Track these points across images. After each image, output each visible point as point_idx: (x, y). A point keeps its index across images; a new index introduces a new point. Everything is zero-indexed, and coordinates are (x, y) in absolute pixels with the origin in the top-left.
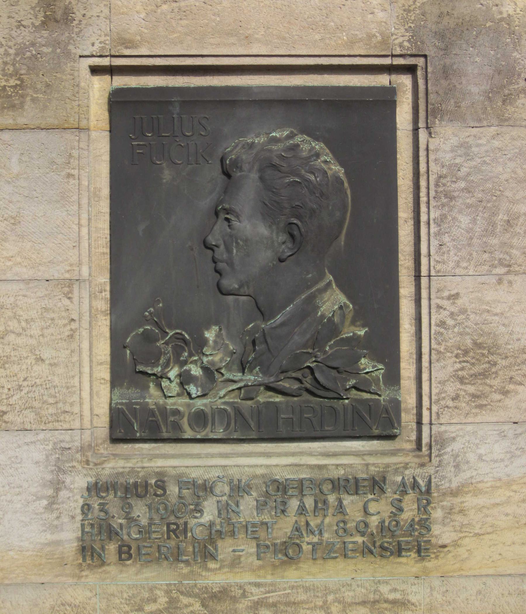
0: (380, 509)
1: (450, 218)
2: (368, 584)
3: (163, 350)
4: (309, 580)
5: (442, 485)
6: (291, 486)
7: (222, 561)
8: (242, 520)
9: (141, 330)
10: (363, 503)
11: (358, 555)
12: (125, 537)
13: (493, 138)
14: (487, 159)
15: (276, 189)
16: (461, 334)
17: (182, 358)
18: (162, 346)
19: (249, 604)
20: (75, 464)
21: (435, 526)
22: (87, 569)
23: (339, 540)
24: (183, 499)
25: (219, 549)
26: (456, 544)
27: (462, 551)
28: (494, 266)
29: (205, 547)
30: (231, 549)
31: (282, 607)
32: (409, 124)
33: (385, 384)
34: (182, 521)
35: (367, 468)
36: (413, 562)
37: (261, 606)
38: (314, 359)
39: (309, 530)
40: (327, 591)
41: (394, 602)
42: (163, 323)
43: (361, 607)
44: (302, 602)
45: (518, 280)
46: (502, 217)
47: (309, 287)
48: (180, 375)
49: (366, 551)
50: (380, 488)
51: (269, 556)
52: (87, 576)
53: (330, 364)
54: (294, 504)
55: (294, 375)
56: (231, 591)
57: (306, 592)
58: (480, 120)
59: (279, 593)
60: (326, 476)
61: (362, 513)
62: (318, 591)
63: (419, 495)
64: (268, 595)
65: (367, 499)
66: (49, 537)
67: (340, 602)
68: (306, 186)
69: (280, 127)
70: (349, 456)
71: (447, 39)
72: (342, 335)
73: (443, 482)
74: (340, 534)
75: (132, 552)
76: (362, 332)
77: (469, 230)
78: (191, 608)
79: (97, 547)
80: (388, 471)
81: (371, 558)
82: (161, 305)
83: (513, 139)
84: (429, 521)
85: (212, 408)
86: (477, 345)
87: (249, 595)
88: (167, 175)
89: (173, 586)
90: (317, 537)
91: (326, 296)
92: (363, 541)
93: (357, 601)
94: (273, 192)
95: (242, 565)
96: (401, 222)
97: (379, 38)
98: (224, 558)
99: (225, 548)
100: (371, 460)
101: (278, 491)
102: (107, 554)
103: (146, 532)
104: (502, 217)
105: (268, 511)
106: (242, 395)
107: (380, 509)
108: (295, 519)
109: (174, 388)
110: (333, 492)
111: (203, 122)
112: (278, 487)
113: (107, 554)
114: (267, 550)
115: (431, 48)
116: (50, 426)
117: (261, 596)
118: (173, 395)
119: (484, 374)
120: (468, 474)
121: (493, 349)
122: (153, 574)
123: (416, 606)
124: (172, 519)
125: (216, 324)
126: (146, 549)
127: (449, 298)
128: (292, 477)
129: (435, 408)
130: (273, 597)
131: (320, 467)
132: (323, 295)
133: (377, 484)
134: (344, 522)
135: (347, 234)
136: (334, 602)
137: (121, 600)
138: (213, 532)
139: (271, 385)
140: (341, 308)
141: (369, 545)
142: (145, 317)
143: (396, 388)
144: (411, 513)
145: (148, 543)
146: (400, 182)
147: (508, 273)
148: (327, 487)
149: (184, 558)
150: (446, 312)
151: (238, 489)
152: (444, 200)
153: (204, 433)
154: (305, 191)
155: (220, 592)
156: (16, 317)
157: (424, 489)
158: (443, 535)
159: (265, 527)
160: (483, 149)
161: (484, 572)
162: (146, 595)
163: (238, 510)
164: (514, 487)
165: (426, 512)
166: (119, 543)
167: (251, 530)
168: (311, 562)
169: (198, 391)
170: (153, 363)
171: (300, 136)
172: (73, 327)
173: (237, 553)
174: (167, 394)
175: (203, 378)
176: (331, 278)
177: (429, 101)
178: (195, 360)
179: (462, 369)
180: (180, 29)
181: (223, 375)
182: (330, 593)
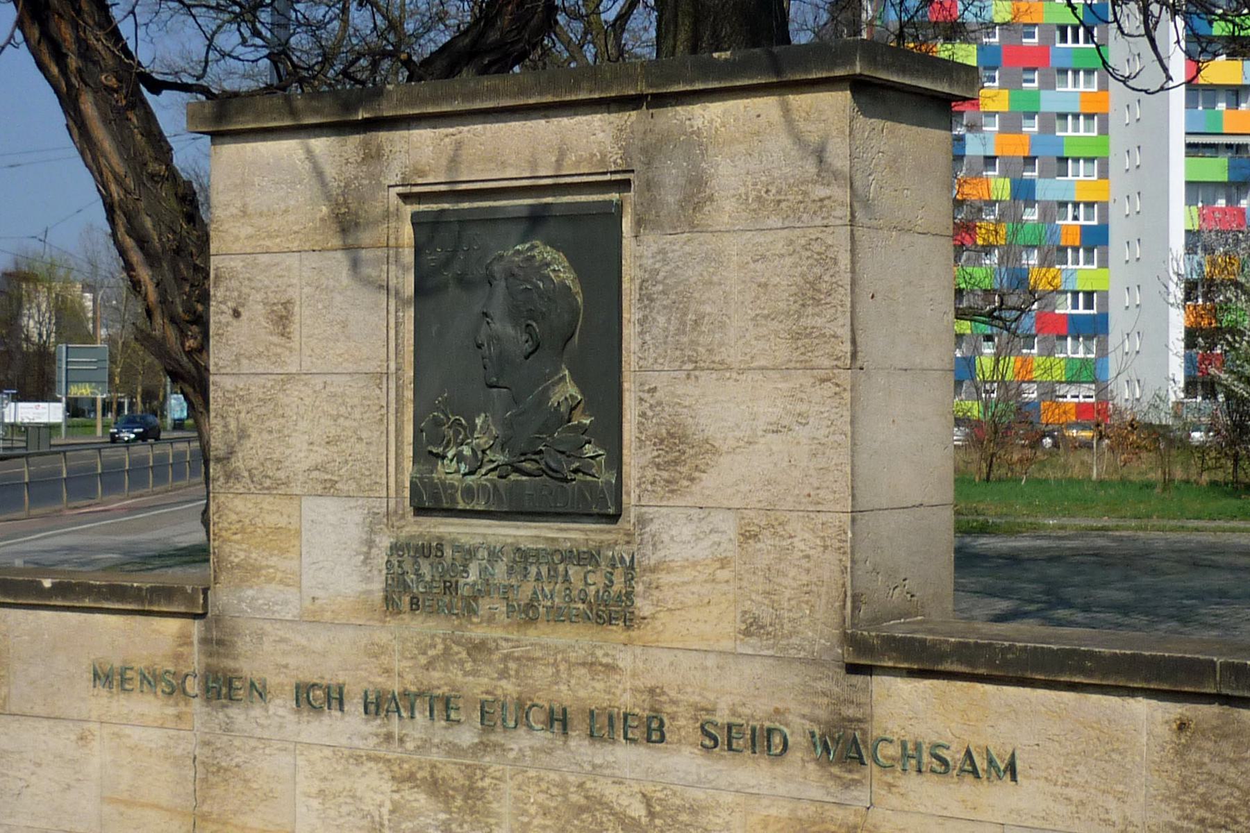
4: (545, 640)
13: (685, 244)
14: (680, 264)
16: (658, 424)
26: (653, 617)
27: (658, 624)
28: (683, 362)
34: (454, 580)
40: (558, 651)
41: (607, 666)
45: (703, 375)
46: (691, 316)
58: (675, 228)
66: (364, 586)
77: (666, 330)
83: (700, 244)
86: (671, 435)
99: (484, 605)
100: (593, 536)
101: (523, 557)
104: (691, 316)
107: (597, 580)
116: (366, 494)
119: (676, 462)
120: (662, 553)
121: (683, 438)
124: (447, 578)
127: (649, 391)
128: (531, 546)
130: (517, 652)
131: (553, 539)
147: (695, 369)
151: (494, 555)
152: (646, 302)
156: (344, 403)
160: (677, 254)
161: (675, 645)
164: (699, 568)
167: (506, 592)
174: (449, 472)
176: (567, 372)
179: (658, 456)
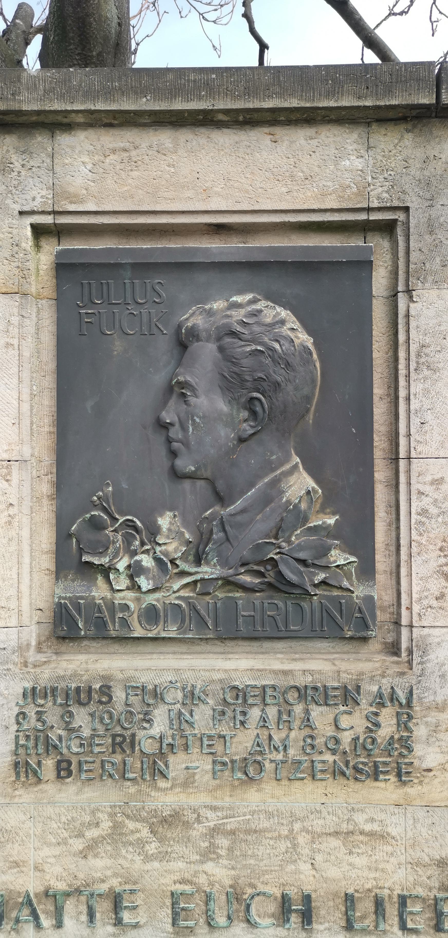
0: (355, 723)
1: (434, 393)
2: (340, 811)
3: (112, 538)
4: (272, 805)
5: (425, 697)
6: (252, 694)
7: (174, 779)
8: (196, 732)
9: (88, 516)
10: (334, 715)
11: (328, 776)
12: (65, 751)
15: (236, 359)
17: (132, 547)
18: (111, 534)
19: (204, 831)
20: (11, 666)
21: (417, 746)
22: (21, 788)
23: (306, 758)
24: (130, 707)
25: (171, 766)
29: (155, 762)
30: (184, 766)
31: (241, 836)
32: (386, 290)
33: (358, 580)
34: (129, 733)
35: (339, 675)
36: (392, 787)
37: (218, 833)
38: (278, 550)
39: (272, 746)
40: (294, 818)
41: (371, 834)
42: (113, 508)
43: (332, 838)
44: (265, 830)
47: (273, 470)
48: (129, 567)
49: (338, 773)
50: (353, 698)
51: (227, 774)
52: (20, 796)
53: (296, 555)
54: (255, 713)
55: (256, 568)
56: (184, 815)
57: (269, 818)
59: (238, 819)
60: (292, 683)
61: (333, 727)
62: (282, 818)
63: (399, 708)
64: (225, 821)
65: (338, 711)
67: (308, 832)
68: (269, 355)
69: (240, 292)
70: (319, 663)
71: (433, 188)
72: (310, 523)
73: (426, 695)
74: (308, 751)
75: (72, 767)
76: (331, 521)
78: (138, 835)
79: (33, 763)
80: (362, 680)
81: (342, 781)
82: (110, 489)
84: (410, 739)
85: (164, 603)
87: (204, 820)
88: (118, 346)
89: (118, 809)
90: (282, 753)
91: (292, 479)
92: (335, 760)
93: (328, 831)
94: (233, 362)
95: (196, 784)
96: (376, 399)
97: (355, 190)
98: (176, 776)
99: (177, 763)
101: (238, 699)
102: (44, 770)
103: (88, 745)
105: (226, 722)
106: (198, 590)
107: (355, 723)
108: (256, 732)
109: (123, 583)
110: (300, 702)
111: (157, 287)
112: (237, 695)
113: (44, 770)
114: (226, 768)
115: (414, 199)
117: (218, 822)
118: (122, 588)
122: (95, 794)
123: (397, 841)
124: (118, 730)
125: (170, 510)
126: (88, 765)
127: (432, 483)
129: (416, 608)
130: (231, 824)
131: (285, 673)
132: (289, 478)
133: (349, 695)
134: (312, 737)
135: (316, 411)
136: (301, 831)
137: (59, 824)
138: (164, 745)
139: (230, 579)
140: (308, 493)
141: (341, 764)
142: (93, 502)
143: (371, 584)
144: (390, 729)
145: (91, 757)
146: (375, 355)
148: (292, 696)
149: (131, 776)
150: (428, 498)
151: (192, 697)
152: (426, 372)
153: (155, 632)
154: (268, 361)
155: (171, 816)
157: (404, 701)
158: (428, 756)
159: (222, 740)
162: (87, 818)
163: (192, 721)
165: (407, 729)
166: (58, 757)
167: (209, 743)
168: (275, 783)
169: (149, 585)
170: (101, 553)
171: (263, 302)
172: (11, 513)
173: (190, 771)
175: (155, 570)
176: (298, 460)
177: (411, 259)
178: (147, 550)
180: (130, 181)
181: (177, 566)
182: (297, 820)
